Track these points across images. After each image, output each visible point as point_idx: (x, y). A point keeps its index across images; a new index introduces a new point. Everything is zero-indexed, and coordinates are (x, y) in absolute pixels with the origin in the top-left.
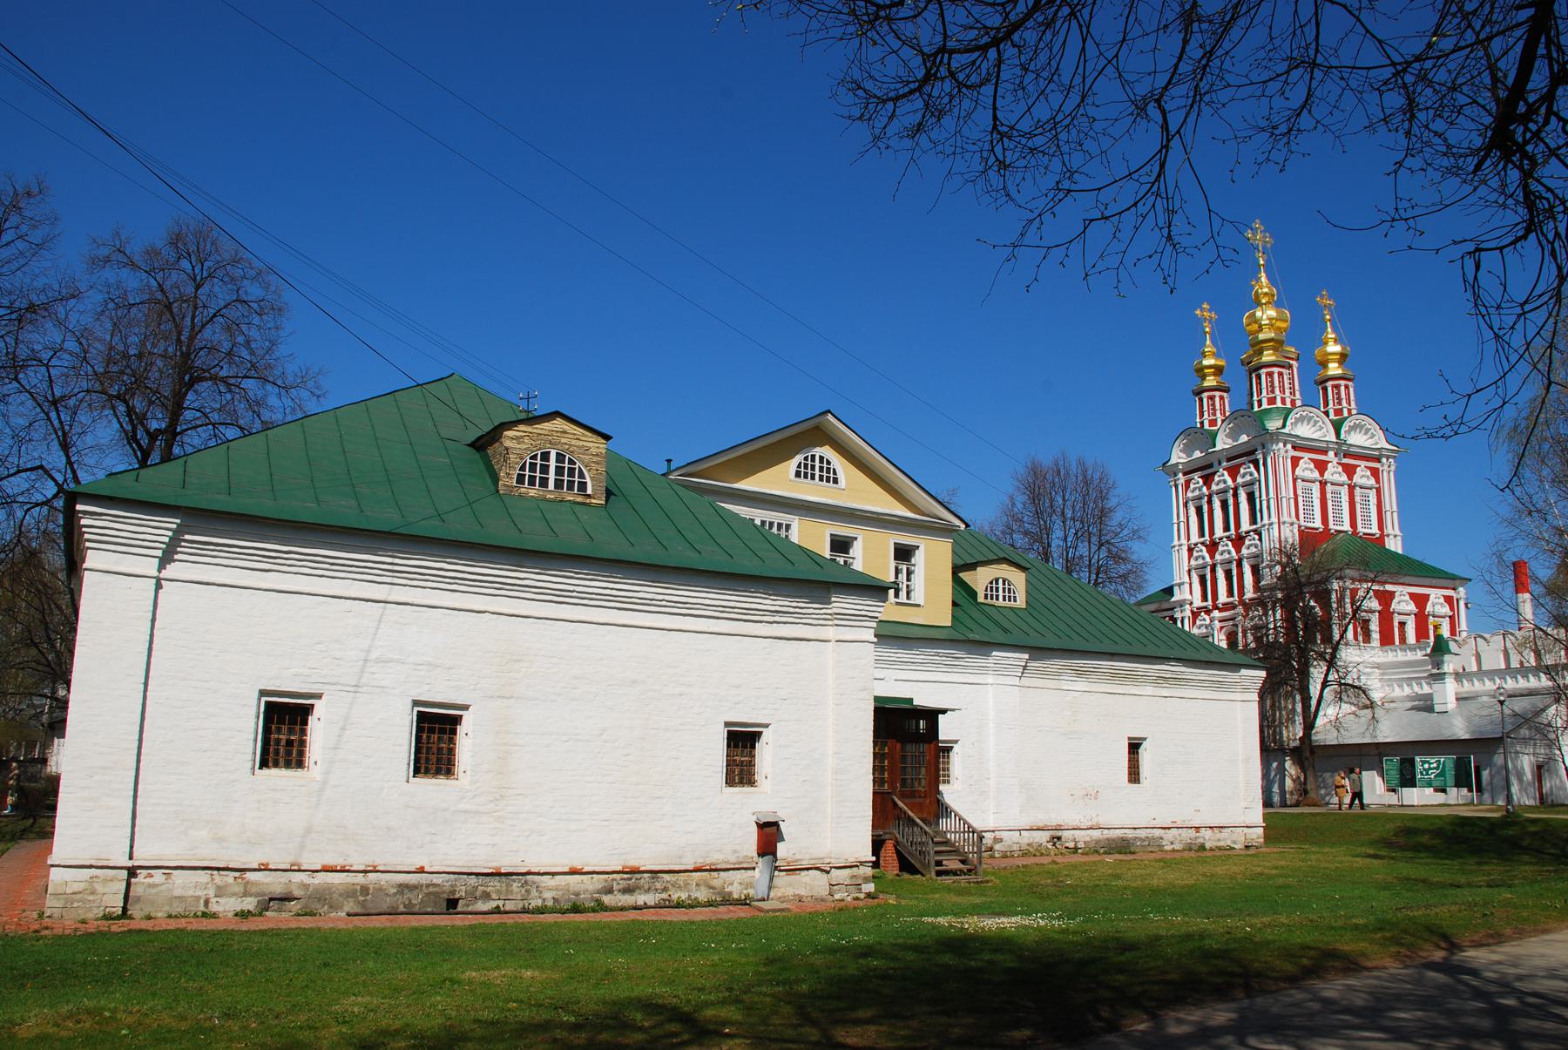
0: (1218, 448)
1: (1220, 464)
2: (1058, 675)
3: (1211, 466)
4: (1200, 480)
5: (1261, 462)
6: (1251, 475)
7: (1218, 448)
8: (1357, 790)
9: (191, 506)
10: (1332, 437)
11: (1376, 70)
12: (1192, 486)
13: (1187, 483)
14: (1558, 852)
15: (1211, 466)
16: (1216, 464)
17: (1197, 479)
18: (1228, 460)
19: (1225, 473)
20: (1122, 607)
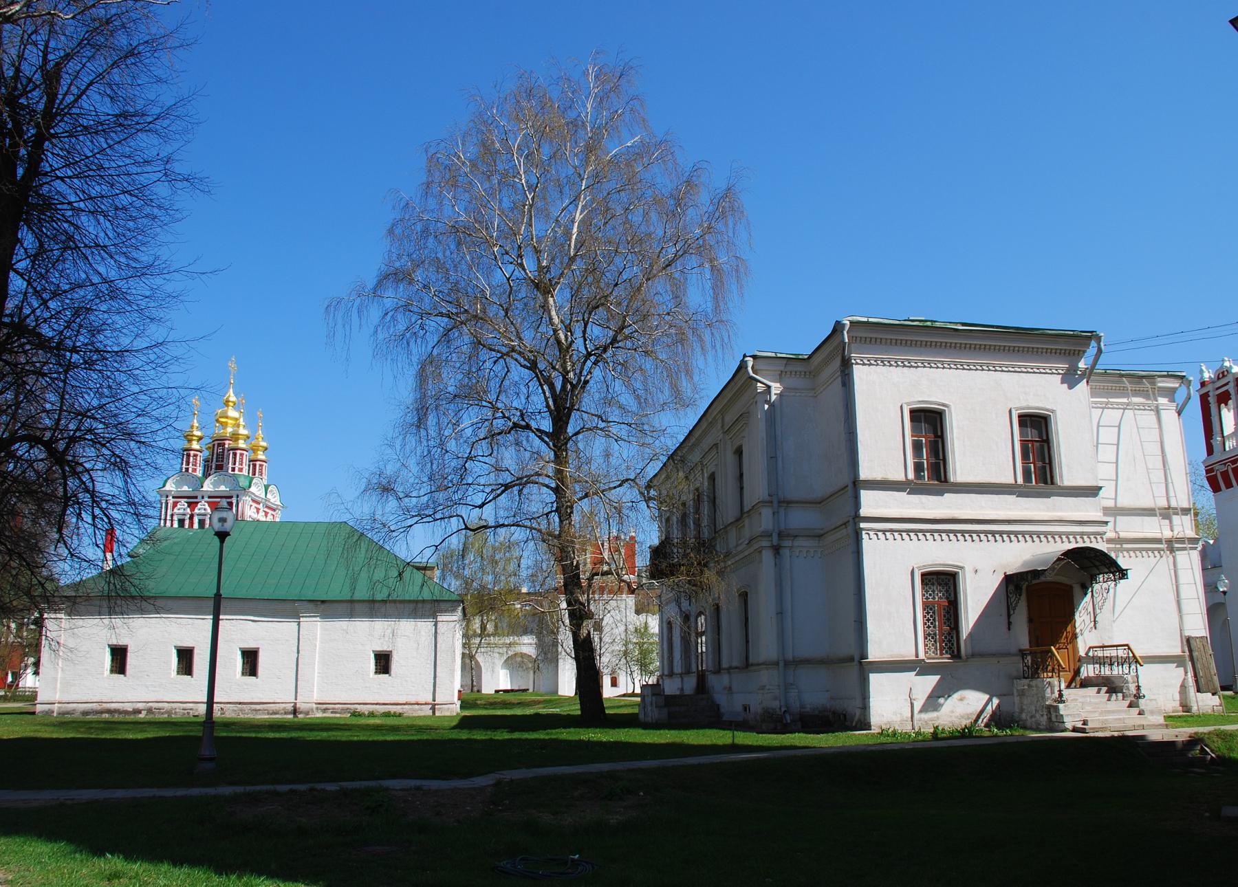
0: (204, 489)
1: (203, 498)
2: (875, 745)
3: (196, 497)
4: (186, 504)
5: (234, 505)
6: (205, 510)
7: (204, 489)
8: (952, 598)
9: (942, 562)
10: (263, 496)
11: (1183, 589)
12: (179, 506)
13: (175, 505)
14: (572, 254)
15: (196, 497)
16: (200, 498)
17: (183, 504)
18: (209, 497)
19: (206, 504)
20: (191, 705)
